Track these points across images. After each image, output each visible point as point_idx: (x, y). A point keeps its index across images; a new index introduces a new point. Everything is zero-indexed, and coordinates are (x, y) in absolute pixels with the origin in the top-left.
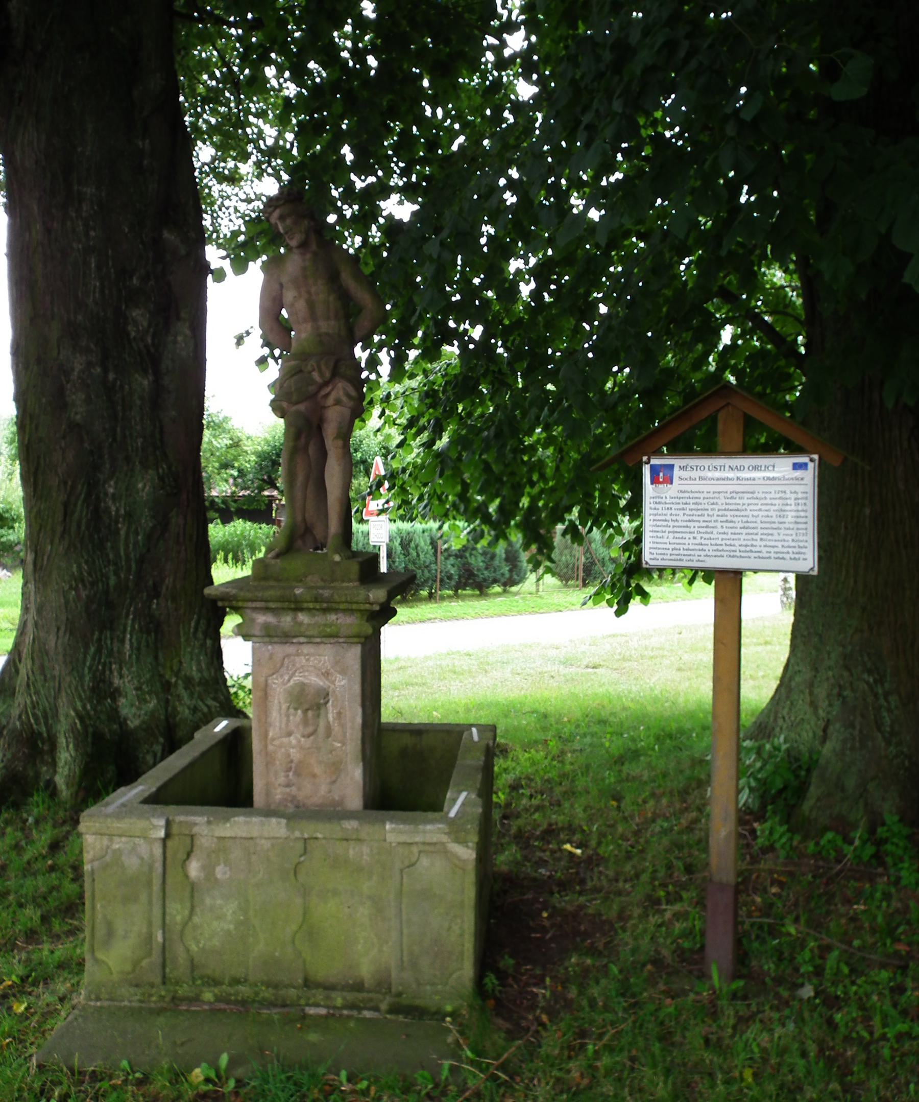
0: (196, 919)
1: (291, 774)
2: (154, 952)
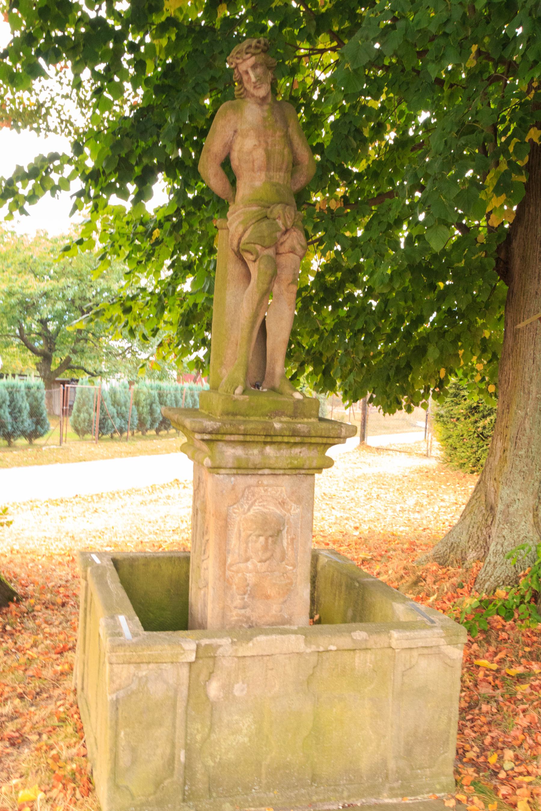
0: (214, 737)
1: (246, 596)
2: (176, 772)
